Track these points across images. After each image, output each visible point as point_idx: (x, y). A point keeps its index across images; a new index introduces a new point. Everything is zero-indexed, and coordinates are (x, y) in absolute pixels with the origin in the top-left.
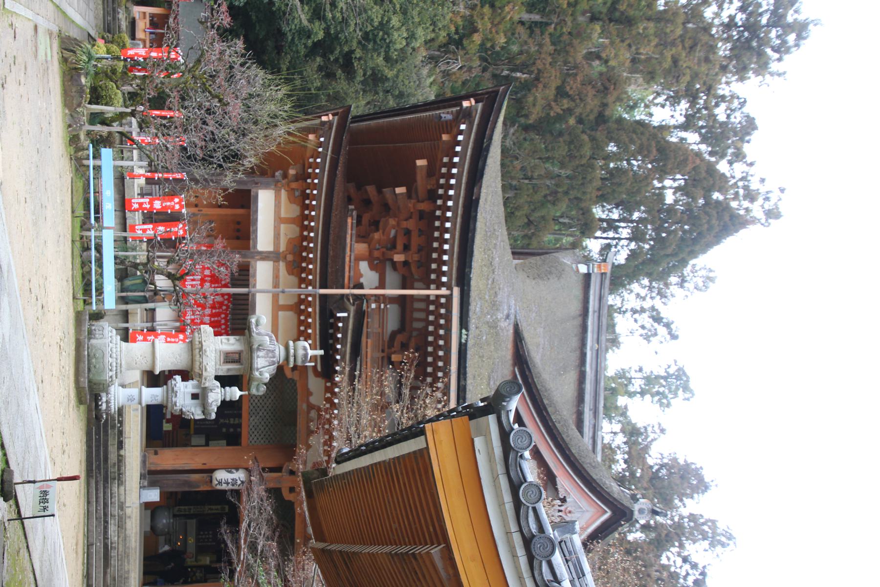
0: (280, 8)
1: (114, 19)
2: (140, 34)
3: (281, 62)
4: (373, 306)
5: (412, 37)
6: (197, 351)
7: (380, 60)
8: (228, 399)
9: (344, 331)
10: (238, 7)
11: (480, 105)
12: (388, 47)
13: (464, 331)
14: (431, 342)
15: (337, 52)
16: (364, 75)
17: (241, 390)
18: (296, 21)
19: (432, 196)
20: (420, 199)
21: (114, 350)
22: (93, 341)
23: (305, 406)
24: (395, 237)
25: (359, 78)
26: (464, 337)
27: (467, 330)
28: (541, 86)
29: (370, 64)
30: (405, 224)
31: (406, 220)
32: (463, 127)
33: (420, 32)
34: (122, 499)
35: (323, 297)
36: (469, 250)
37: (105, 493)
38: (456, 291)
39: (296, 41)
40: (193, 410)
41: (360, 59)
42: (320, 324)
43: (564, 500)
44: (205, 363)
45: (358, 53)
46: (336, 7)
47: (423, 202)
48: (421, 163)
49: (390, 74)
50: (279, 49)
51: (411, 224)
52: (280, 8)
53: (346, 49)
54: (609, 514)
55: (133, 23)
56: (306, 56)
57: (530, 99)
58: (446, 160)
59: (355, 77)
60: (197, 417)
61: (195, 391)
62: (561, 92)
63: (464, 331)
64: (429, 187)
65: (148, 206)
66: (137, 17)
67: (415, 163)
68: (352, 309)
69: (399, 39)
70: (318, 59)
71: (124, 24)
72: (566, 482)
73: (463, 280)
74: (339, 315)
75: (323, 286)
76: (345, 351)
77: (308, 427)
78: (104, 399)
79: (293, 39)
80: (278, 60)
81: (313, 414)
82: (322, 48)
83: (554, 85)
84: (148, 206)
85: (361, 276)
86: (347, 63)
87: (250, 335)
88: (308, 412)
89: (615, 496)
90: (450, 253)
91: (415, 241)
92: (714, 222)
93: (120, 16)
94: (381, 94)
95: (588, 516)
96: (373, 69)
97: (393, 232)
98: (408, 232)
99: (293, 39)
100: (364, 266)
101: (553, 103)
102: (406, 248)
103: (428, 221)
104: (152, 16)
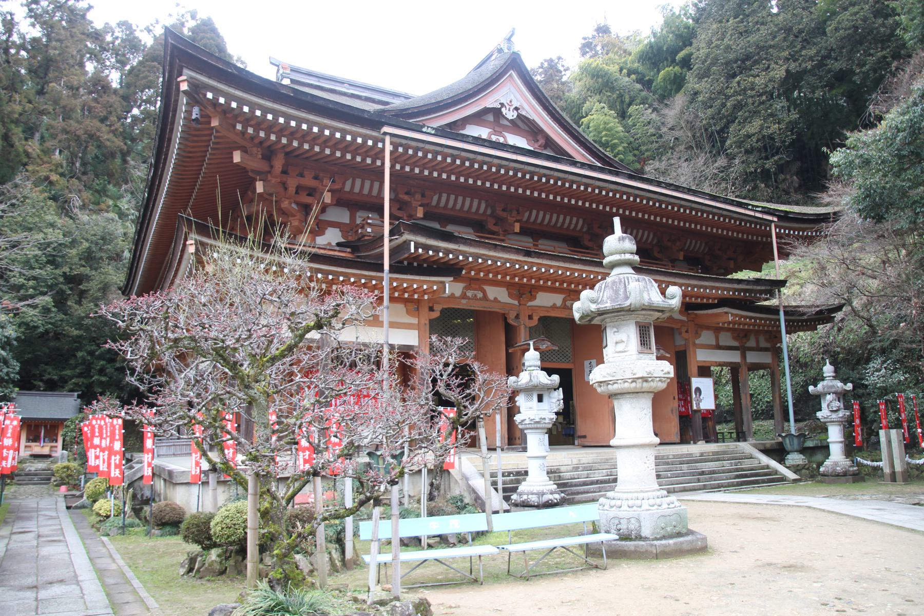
0: (23, 332)
1: (36, 475)
2: (46, 451)
3: (71, 334)
4: (369, 230)
5: (52, 225)
6: (645, 384)
7: (74, 252)
8: (539, 363)
9: (426, 248)
10: (21, 368)
11: (185, 71)
12: (60, 245)
13: (424, 130)
14: (420, 171)
15: (64, 287)
16: (84, 266)
17: (528, 350)
18: (35, 319)
19: (269, 153)
20: (267, 169)
21: (651, 501)
22: (646, 532)
23: (464, 301)
24: (297, 204)
25: (87, 271)
26: (429, 130)
27: (424, 126)
28: (98, 134)
29: (76, 260)
30: (292, 190)
31: (286, 189)
32: (210, 95)
33: (49, 218)
34: (570, 468)
35: (393, 269)
36: (345, 110)
37: (576, 485)
38: (386, 129)
39: (53, 321)
40: (554, 400)
41: (71, 269)
42: (412, 274)
43: (502, 105)
44: (661, 374)
45: (66, 269)
46: (23, 285)
47: (272, 167)
48: (237, 157)
49: (86, 245)
50: (58, 336)
51: (292, 183)
52: (23, 332)
53: (61, 279)
54: (511, 72)
55: (36, 457)
56: (66, 314)
57: (108, 143)
58: (239, 127)
59: (87, 275)
60: (562, 397)
61: (535, 398)
62: (103, 120)
63: (424, 130)
64: (260, 156)
65: (307, 453)
66: (29, 453)
67: (237, 165)
68: (407, 236)
69: (55, 236)
70: (69, 303)
71: (40, 465)
72: (490, 101)
73: (373, 122)
74: (413, 251)
75: (380, 268)
76: (445, 249)
77: (480, 299)
78: (551, 497)
79: (50, 323)
80: (69, 337)
81: (470, 294)
82: (60, 302)
83: (98, 124)
84: (307, 453)
85: (329, 244)
86: (74, 280)
87: (601, 313)
88: (468, 298)
89: (502, 62)
90: (344, 132)
91: (308, 181)
92: (208, 35)
93: (33, 469)
94: (102, 254)
95: (512, 89)
96: (80, 259)
97: (294, 206)
98: (298, 189)
99: (50, 323)
100: (321, 240)
101: (113, 128)
102: (312, 192)
103: (295, 161)
104: (28, 440)
